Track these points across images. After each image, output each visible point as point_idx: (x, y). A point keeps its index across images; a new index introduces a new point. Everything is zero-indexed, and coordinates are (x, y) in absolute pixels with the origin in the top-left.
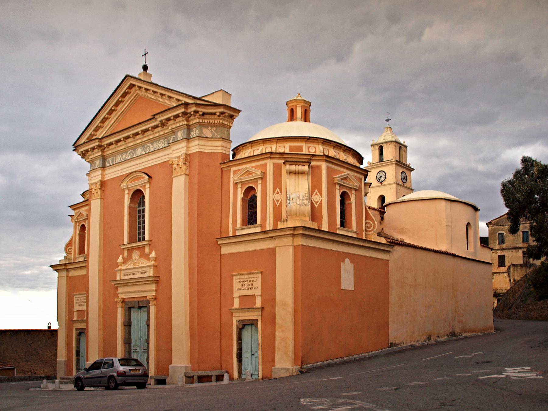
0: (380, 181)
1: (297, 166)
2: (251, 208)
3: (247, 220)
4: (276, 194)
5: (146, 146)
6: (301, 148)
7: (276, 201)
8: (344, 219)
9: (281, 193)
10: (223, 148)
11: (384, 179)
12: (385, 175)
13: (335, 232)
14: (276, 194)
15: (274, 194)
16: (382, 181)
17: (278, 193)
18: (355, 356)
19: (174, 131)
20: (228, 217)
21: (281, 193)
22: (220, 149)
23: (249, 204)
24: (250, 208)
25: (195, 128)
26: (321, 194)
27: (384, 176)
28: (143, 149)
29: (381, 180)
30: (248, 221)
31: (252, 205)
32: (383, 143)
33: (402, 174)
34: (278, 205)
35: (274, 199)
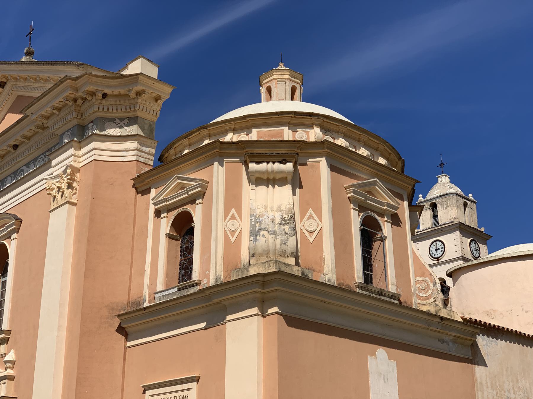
0: (436, 256)
1: (271, 163)
2: (186, 253)
3: (178, 276)
4: (230, 220)
5: (18, 172)
6: (281, 134)
7: (228, 232)
8: (371, 271)
9: (241, 219)
10: (140, 153)
11: (442, 253)
12: (442, 246)
13: (281, 139)
14: (230, 220)
15: (225, 219)
16: (439, 255)
17: (233, 217)
18: (520, 381)
19: (226, 303)
20: (142, 274)
21: (241, 219)
22: (134, 154)
23: (181, 247)
24: (184, 254)
25: (92, 122)
26: (320, 218)
27: (442, 248)
28: (15, 177)
29: (437, 255)
30: (179, 278)
31: (187, 248)
32: (435, 198)
33: (472, 243)
34: (233, 240)
35: (226, 229)
